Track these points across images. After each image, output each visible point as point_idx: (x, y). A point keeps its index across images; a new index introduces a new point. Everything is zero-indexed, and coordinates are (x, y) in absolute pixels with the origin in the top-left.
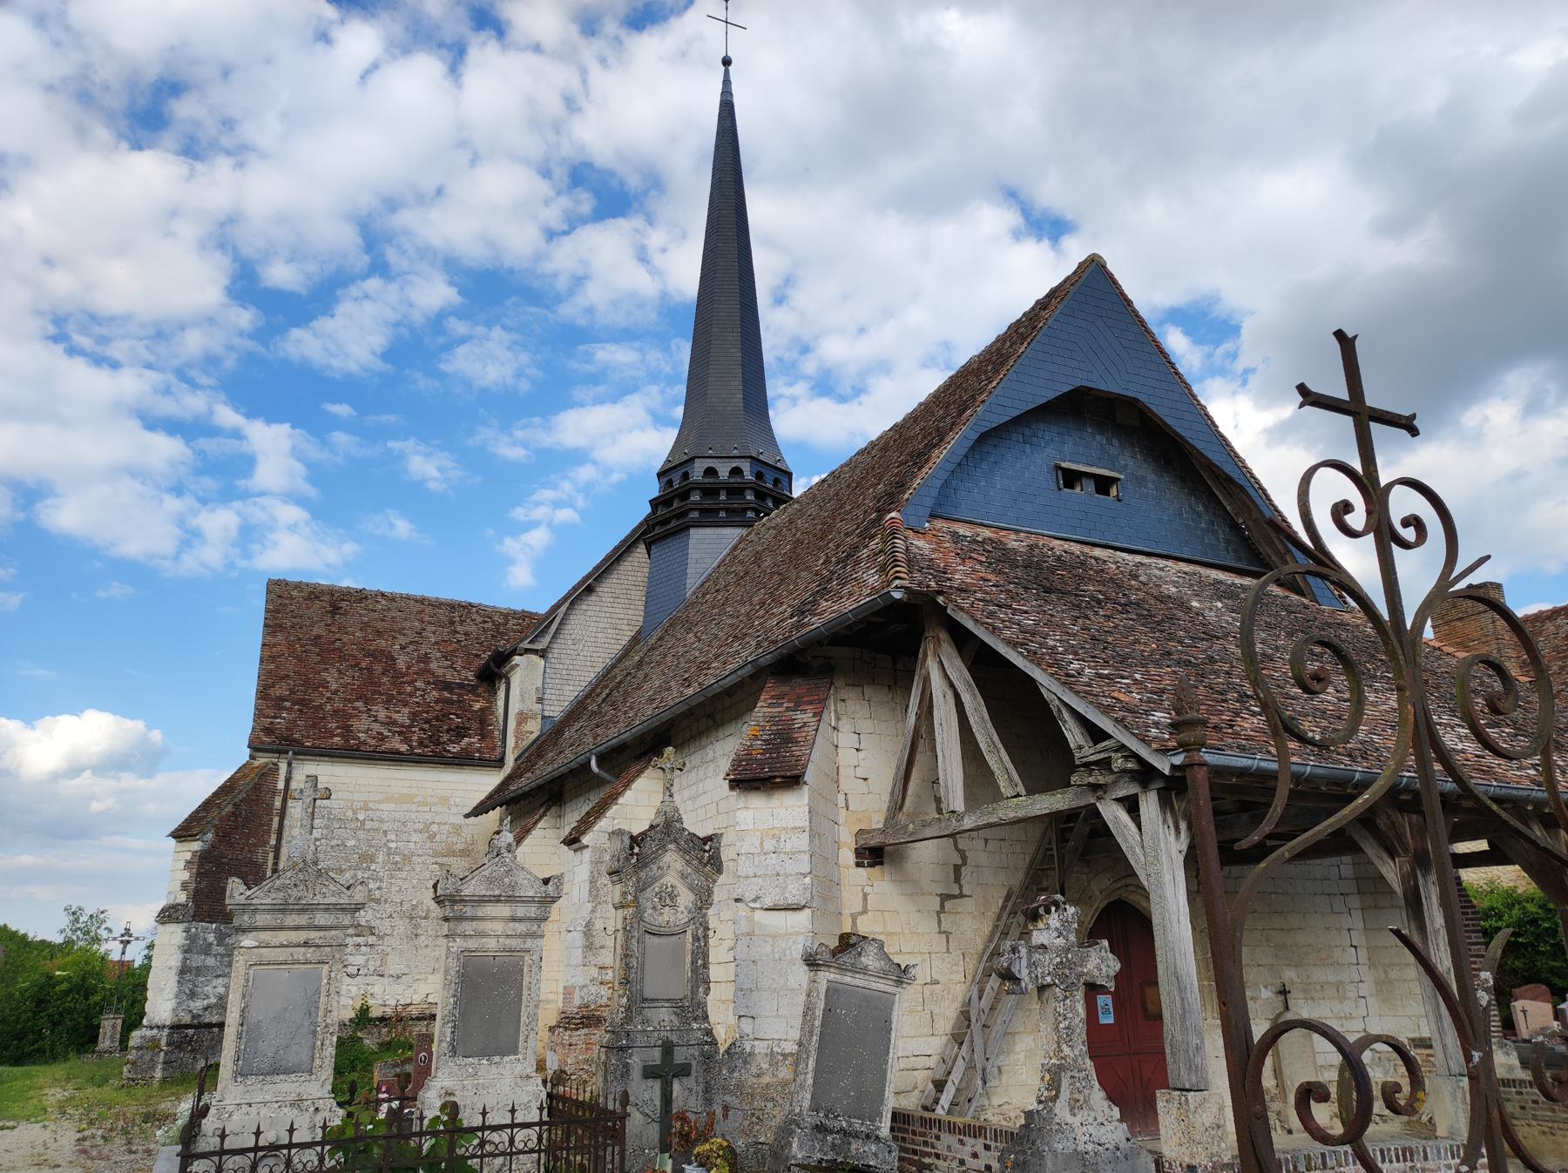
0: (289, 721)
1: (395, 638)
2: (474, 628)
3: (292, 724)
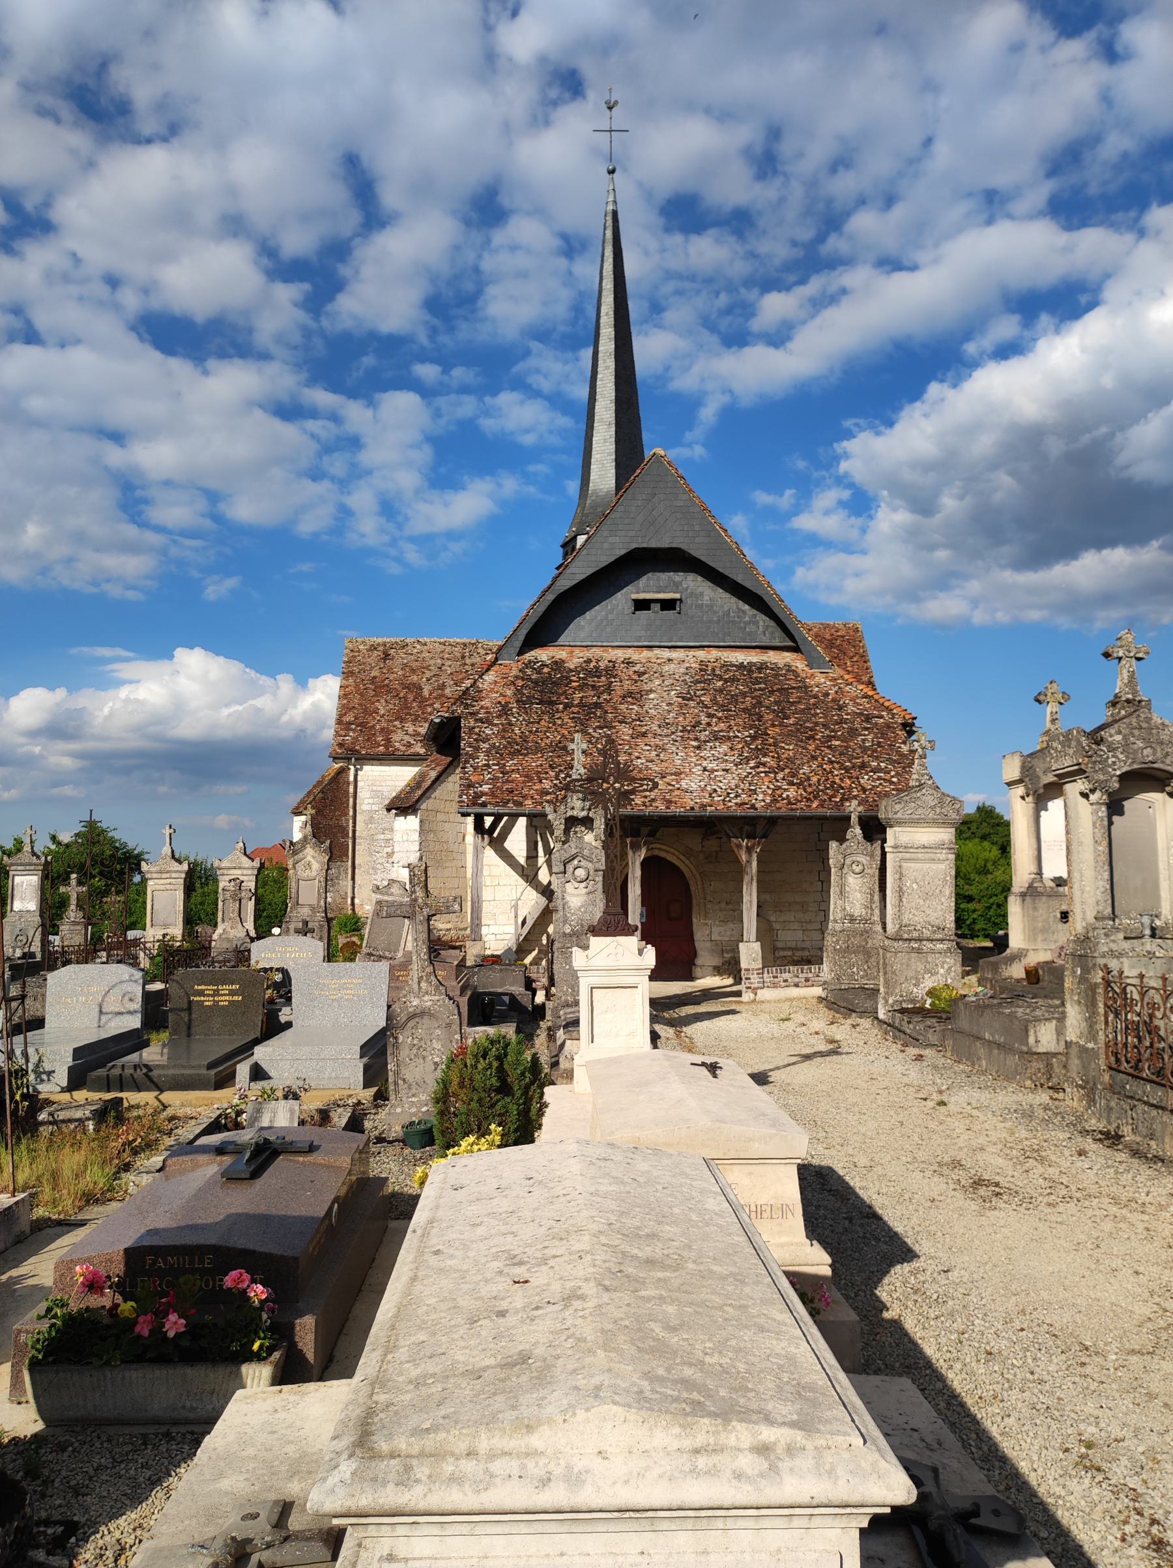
0: (354, 738)
1: (424, 673)
2: (479, 659)
3: (355, 739)
